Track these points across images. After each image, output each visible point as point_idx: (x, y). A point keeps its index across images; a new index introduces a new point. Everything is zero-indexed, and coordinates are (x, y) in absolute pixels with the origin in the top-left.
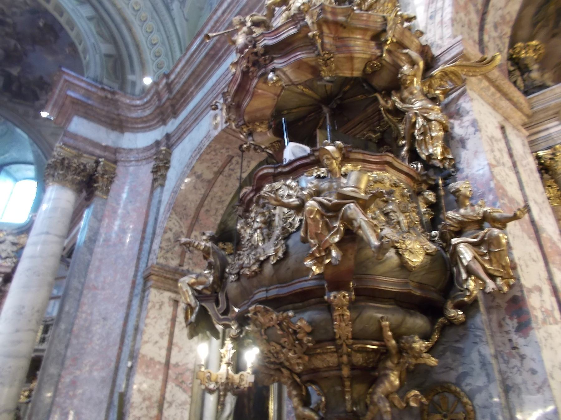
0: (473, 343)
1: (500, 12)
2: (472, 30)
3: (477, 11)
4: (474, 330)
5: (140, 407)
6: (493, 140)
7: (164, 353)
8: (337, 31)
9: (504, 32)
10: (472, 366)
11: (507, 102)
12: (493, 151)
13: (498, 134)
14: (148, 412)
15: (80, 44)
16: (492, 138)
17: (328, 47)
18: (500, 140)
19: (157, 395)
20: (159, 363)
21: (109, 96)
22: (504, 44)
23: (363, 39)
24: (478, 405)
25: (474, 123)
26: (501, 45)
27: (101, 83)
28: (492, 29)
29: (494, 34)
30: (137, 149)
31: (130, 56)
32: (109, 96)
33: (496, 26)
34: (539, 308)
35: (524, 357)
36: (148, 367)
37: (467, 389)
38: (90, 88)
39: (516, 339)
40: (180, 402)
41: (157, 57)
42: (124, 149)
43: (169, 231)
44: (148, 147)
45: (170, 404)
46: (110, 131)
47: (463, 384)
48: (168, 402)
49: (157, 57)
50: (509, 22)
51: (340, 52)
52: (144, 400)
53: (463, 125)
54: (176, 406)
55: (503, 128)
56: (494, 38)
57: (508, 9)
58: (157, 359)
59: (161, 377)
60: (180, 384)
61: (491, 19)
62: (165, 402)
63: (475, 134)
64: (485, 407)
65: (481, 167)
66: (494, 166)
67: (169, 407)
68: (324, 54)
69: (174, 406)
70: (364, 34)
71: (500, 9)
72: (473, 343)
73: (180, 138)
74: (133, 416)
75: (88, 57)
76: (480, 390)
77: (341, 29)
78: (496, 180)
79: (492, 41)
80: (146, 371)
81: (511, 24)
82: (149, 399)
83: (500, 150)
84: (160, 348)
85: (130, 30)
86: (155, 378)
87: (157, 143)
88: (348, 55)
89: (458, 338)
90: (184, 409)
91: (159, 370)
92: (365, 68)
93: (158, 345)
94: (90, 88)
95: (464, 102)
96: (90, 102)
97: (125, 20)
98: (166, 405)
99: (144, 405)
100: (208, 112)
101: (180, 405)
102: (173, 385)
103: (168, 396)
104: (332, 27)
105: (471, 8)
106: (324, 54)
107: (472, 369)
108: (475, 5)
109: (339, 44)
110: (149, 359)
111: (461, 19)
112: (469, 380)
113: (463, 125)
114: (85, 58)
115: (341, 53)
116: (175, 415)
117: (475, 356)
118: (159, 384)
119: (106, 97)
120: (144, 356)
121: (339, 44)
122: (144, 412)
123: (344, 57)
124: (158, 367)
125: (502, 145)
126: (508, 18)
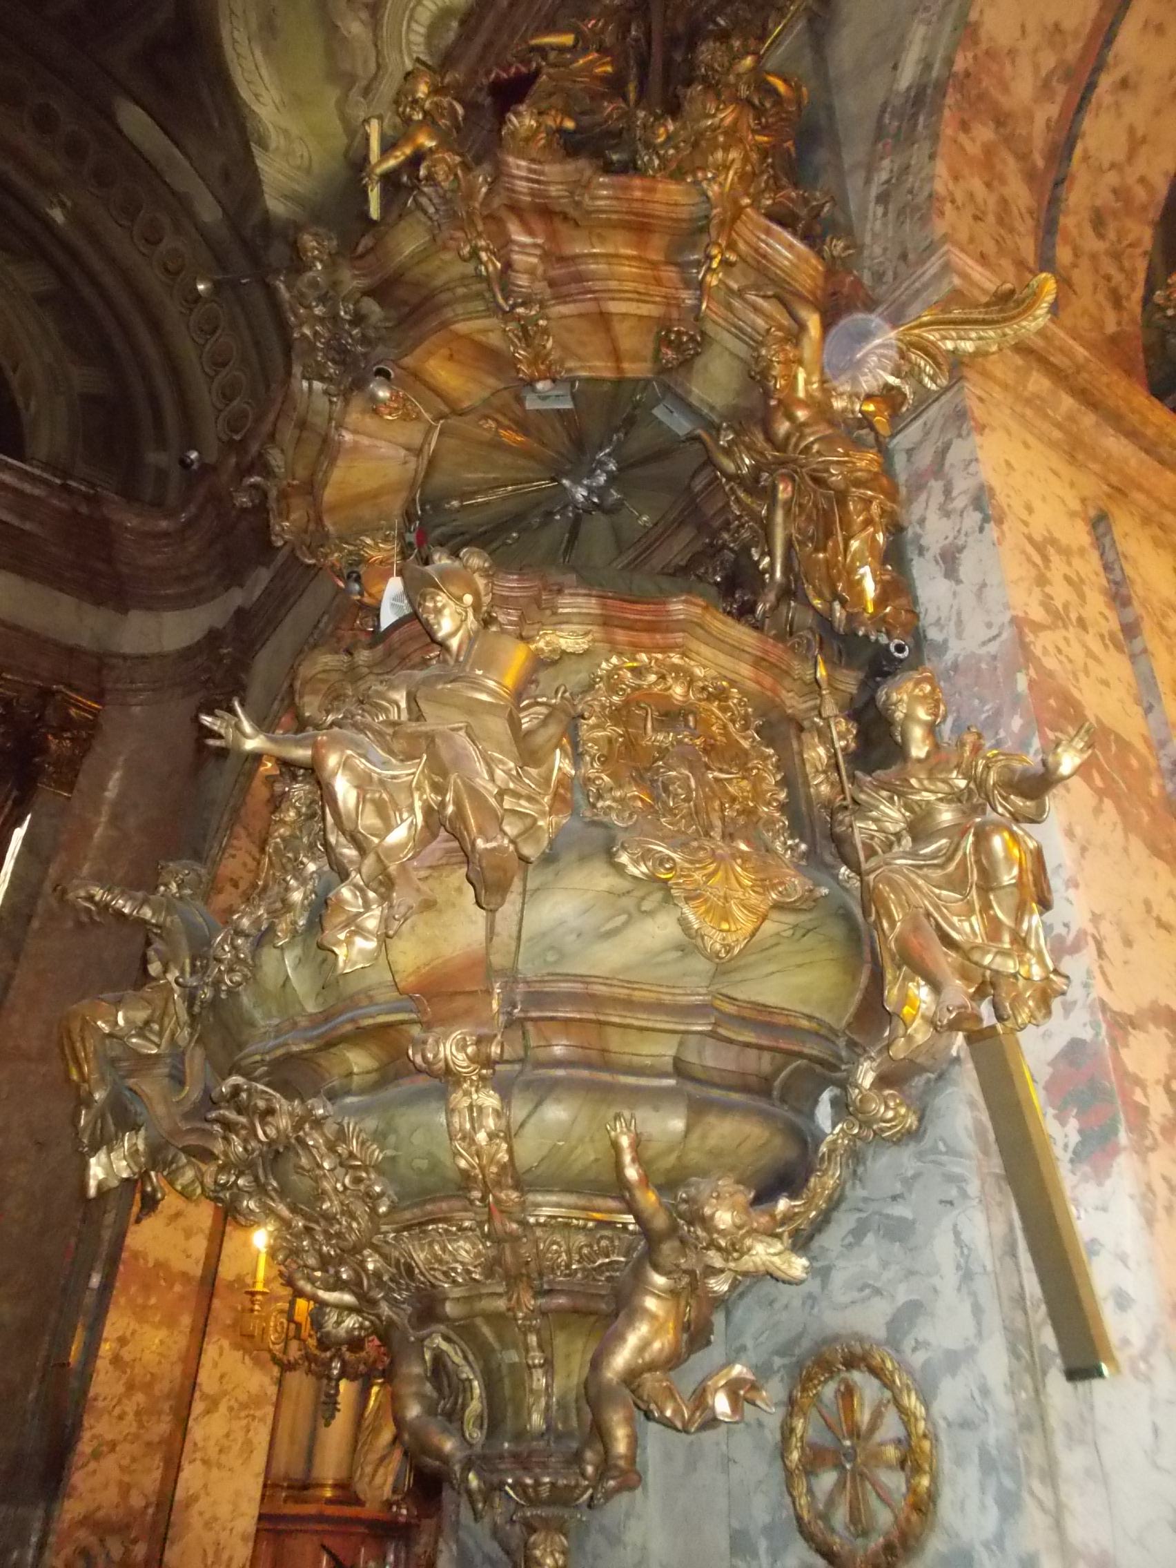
0: (941, 1202)
1: (1112, 178)
2: (1011, 230)
3: (1031, 177)
4: (944, 1158)
5: (117, 1411)
6: (1051, 551)
7: (199, 1246)
8: (552, 236)
9: (1131, 237)
10: (935, 1280)
11: (1124, 441)
12: (1042, 581)
13: (1079, 535)
14: (141, 1426)
15: (15, 370)
16: (1044, 546)
17: (523, 281)
18: (1082, 551)
19: (172, 1374)
20: (185, 1278)
21: (84, 509)
22: (1130, 275)
23: (639, 258)
24: (945, 1418)
25: (982, 499)
26: (1118, 277)
27: (66, 474)
28: (1089, 231)
29: (1093, 244)
30: (161, 656)
31: (154, 401)
32: (84, 509)
33: (1098, 221)
34: (1158, 1082)
35: (1096, 1247)
36: (147, 1288)
37: (918, 1359)
38: (27, 488)
39: (1074, 1187)
40: (243, 1398)
41: (227, 398)
42: (125, 657)
43: (229, 888)
44: (189, 648)
45: (213, 1403)
46: (86, 606)
47: (908, 1344)
48: (205, 1397)
49: (227, 398)
50: (1144, 208)
51: (562, 299)
52: (131, 1387)
53: (950, 507)
54: (231, 1409)
55: (1099, 523)
56: (1094, 257)
57: (1141, 167)
58: (179, 1264)
59: (186, 1320)
60: (247, 1341)
61: (1077, 198)
62: (197, 1394)
63: (981, 530)
64: (966, 1424)
65: (994, 631)
66: (1037, 627)
67: (208, 1412)
68: (513, 307)
69: (223, 1408)
70: (641, 244)
71: (1113, 166)
72: (941, 1202)
73: (273, 623)
74: (94, 1437)
75: (33, 404)
76: (954, 1361)
77: (563, 229)
78: (1040, 668)
79: (1085, 263)
80: (140, 1301)
81: (1154, 214)
82: (148, 1387)
83: (1076, 584)
84: (188, 1234)
85: (156, 326)
86: (170, 1322)
87: (213, 638)
88: (589, 307)
89: (898, 1188)
90: (254, 1417)
91: (182, 1297)
92: (657, 351)
93: (181, 1222)
94: (27, 488)
95: (960, 436)
96: (28, 526)
97: (141, 300)
98: (198, 1407)
99: (130, 1407)
100: (578, 595)
101: (244, 1406)
102: (226, 1343)
103: (207, 1380)
104: (538, 226)
105: (1010, 166)
106: (513, 307)
107: (935, 1291)
108: (1023, 157)
109: (557, 272)
110: (151, 1264)
111: (971, 196)
112: (923, 1330)
113: (950, 507)
114: (27, 407)
115: (566, 303)
116: (227, 1435)
117: (943, 1249)
118: (180, 1341)
119: (76, 512)
120: (136, 1255)
121: (557, 272)
122: (129, 1424)
123: (580, 316)
124: (178, 1288)
125: (1089, 567)
126: (1141, 194)
